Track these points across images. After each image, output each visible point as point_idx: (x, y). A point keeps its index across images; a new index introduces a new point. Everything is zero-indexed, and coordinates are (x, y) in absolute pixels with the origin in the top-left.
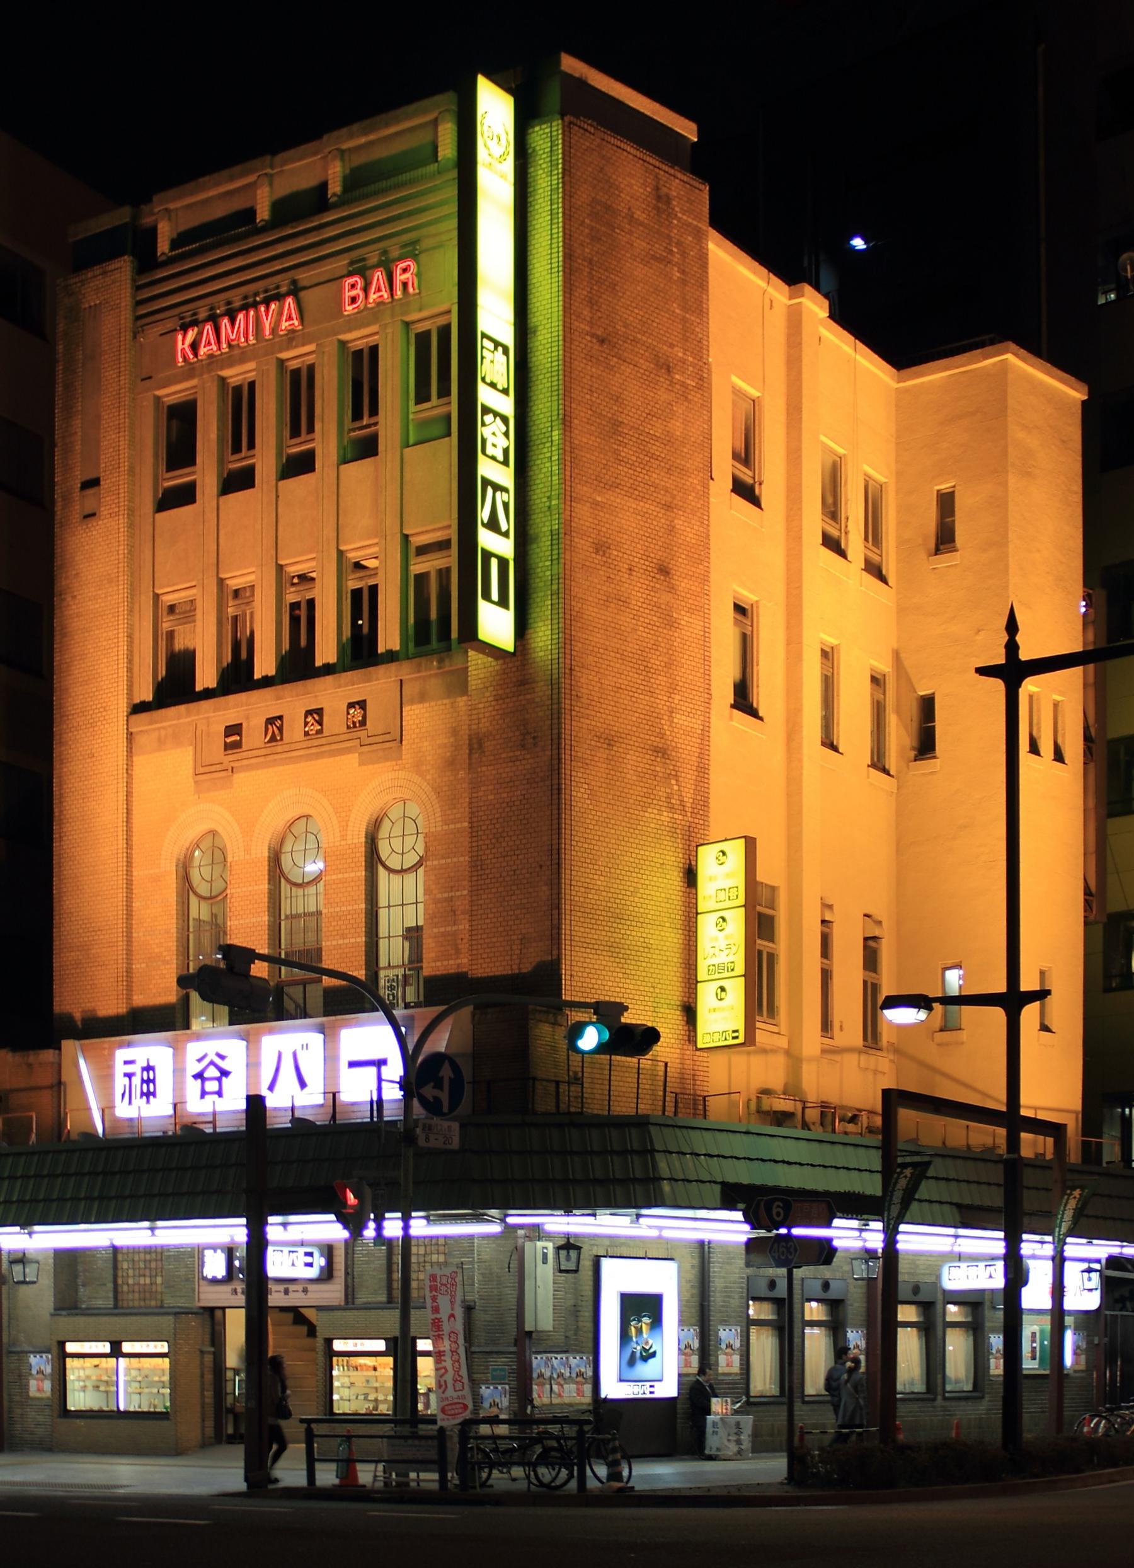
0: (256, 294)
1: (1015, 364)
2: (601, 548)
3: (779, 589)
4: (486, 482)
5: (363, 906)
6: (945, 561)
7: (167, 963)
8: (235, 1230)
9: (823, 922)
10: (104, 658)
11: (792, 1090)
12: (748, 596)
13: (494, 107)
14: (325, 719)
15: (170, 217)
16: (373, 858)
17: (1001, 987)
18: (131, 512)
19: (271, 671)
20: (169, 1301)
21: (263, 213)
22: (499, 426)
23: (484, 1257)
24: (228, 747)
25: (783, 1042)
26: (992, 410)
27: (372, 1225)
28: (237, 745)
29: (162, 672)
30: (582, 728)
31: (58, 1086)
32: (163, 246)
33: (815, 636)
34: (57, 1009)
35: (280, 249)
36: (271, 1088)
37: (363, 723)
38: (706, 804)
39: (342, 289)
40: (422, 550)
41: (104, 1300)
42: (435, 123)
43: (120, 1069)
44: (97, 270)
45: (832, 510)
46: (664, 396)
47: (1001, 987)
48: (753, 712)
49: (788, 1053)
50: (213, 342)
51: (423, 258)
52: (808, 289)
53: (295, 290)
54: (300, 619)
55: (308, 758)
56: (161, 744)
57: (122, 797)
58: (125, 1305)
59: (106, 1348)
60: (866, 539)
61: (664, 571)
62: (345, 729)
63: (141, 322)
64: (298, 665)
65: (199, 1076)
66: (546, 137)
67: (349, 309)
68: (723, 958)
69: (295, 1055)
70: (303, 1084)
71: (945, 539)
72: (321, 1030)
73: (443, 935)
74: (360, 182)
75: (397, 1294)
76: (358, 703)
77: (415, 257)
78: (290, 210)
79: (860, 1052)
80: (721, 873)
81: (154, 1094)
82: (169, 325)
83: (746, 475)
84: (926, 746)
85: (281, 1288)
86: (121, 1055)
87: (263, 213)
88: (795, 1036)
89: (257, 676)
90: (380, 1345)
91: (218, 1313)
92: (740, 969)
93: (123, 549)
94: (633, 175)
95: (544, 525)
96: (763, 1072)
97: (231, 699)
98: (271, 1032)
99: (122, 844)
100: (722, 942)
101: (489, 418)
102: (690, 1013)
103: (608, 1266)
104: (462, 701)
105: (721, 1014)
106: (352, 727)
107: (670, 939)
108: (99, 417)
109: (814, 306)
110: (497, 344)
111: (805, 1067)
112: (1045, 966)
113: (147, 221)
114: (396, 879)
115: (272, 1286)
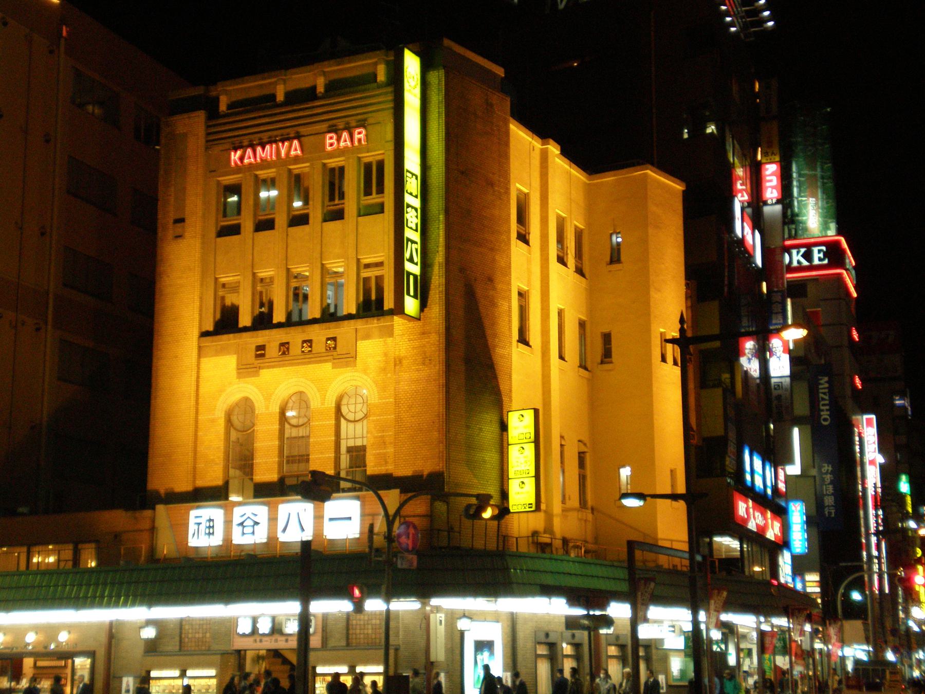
0: (277, 136)
1: (652, 174)
4: (408, 240)
5: (333, 438)
7: (216, 464)
10: (185, 308)
11: (549, 529)
14: (314, 345)
15: (226, 95)
18: (203, 236)
20: (215, 647)
21: (280, 97)
22: (413, 213)
28: (263, 355)
29: (218, 316)
32: (223, 107)
33: (555, 305)
36: (284, 530)
37: (335, 348)
39: (324, 139)
42: (376, 64)
44: (185, 116)
51: (369, 128)
52: (551, 141)
53: (298, 137)
59: (177, 673)
62: (324, 350)
63: (210, 143)
65: (241, 524)
66: (437, 77)
70: (303, 530)
73: (378, 454)
74: (336, 87)
77: (364, 127)
81: (213, 533)
82: (227, 146)
84: (607, 354)
86: (193, 513)
87: (280, 97)
89: (275, 321)
91: (242, 653)
97: (260, 333)
98: (283, 502)
101: (409, 209)
106: (328, 349)
108: (185, 188)
109: (554, 149)
110: (413, 174)
113: (214, 94)
114: (351, 425)
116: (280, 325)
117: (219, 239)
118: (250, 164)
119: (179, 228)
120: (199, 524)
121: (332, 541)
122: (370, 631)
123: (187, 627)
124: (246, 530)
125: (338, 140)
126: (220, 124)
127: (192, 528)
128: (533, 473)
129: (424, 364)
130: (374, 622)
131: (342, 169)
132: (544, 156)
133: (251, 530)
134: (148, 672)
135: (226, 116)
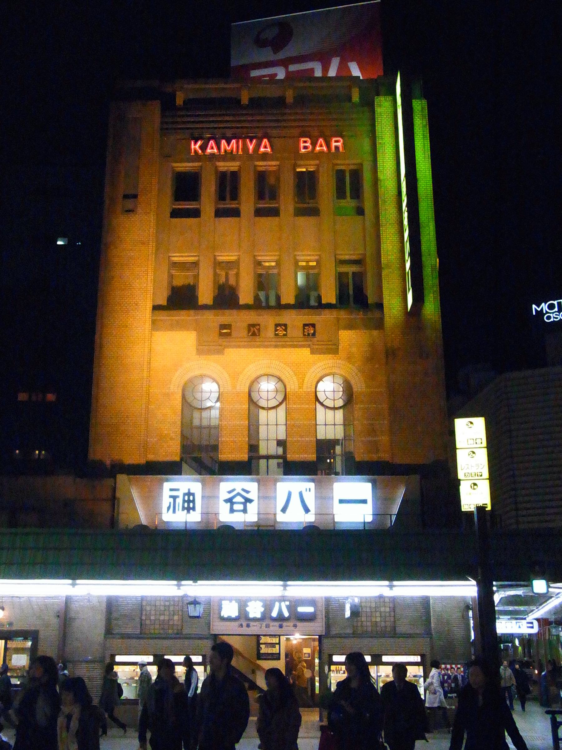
8: (467, 589)
19: (292, 301)
23: (437, 609)
28: (229, 334)
31: (113, 500)
36: (284, 510)
37: (314, 334)
50: (268, 146)
51: (346, 138)
53: (266, 136)
55: (276, 346)
58: (147, 632)
63: (164, 130)
65: (230, 501)
67: (303, 151)
69: (301, 494)
73: (370, 442)
76: (311, 324)
85: (277, 624)
86: (167, 486)
87: (245, 100)
90: (418, 659)
92: (486, 474)
113: (169, 90)
116: (247, 307)
117: (172, 219)
118: (213, 155)
119: (129, 204)
121: (168, 522)
122: (378, 619)
123: (148, 608)
124: (236, 507)
125: (314, 144)
126: (198, 116)
127: (166, 501)
130: (382, 609)
131: (235, 175)
133: (241, 507)
134: (113, 656)
135: (180, 109)
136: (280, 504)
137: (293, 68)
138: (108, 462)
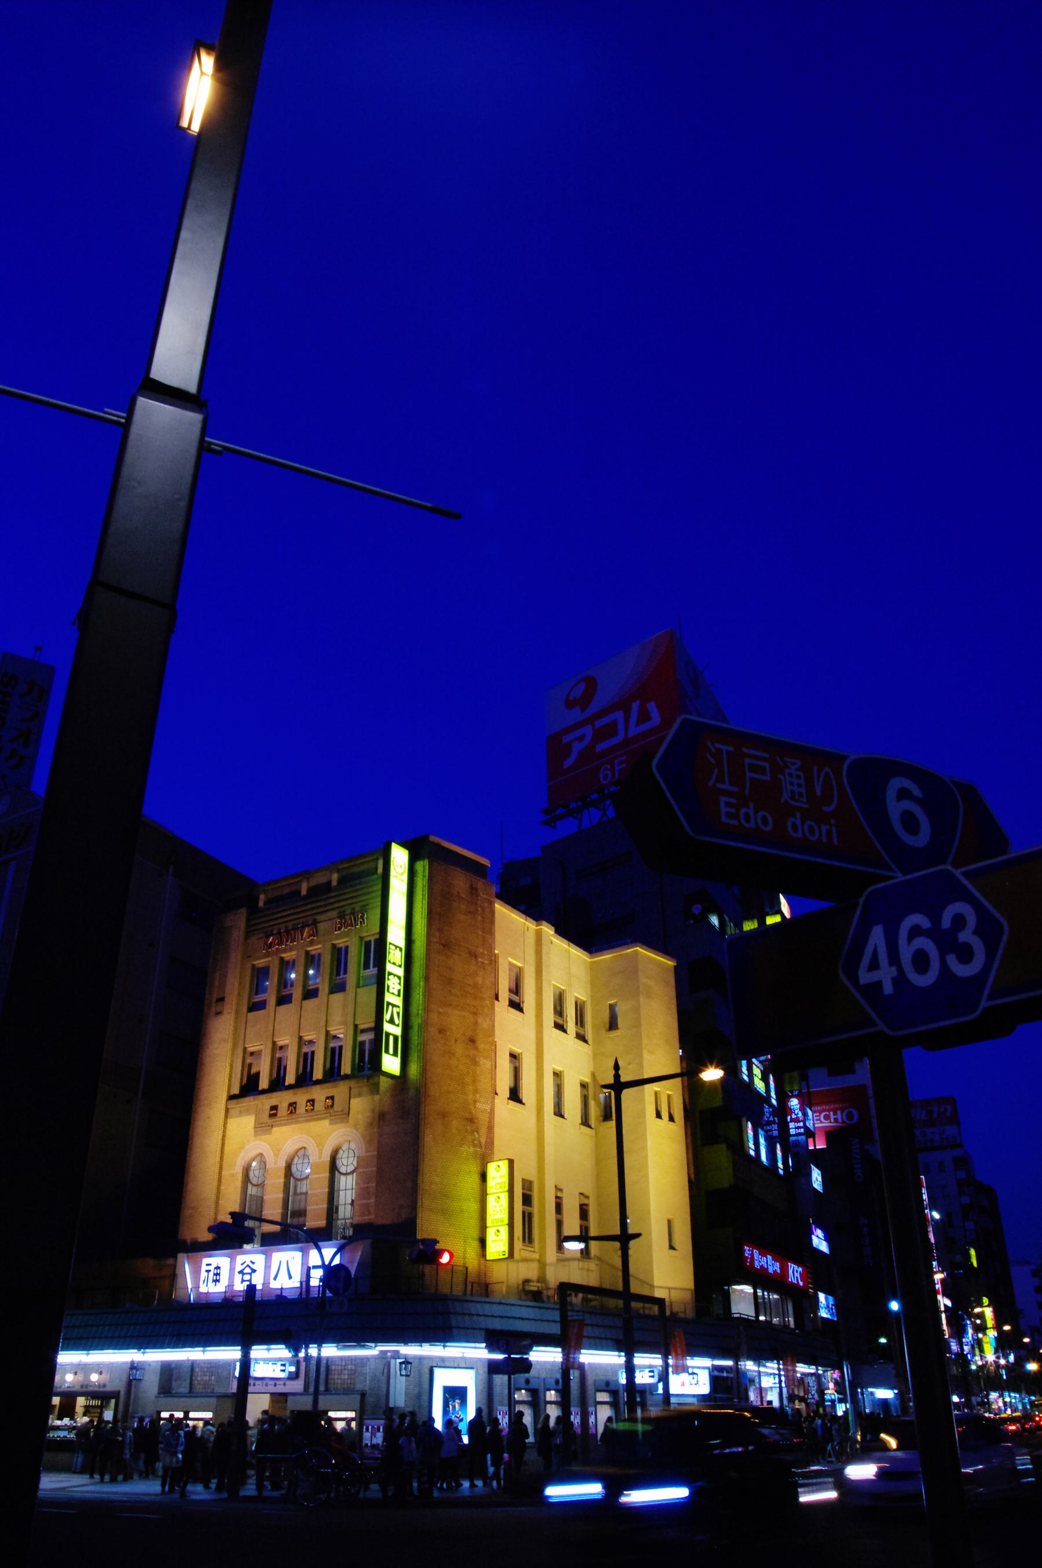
2: (441, 1031)
3: (533, 1047)
4: (389, 1004)
6: (614, 1034)
8: (231, 1354)
9: (557, 1197)
11: (542, 1279)
12: (517, 1050)
13: (399, 856)
16: (333, 1167)
17: (617, 1231)
18: (237, 1012)
24: (271, 1116)
25: (536, 1256)
26: (632, 971)
27: (303, 1351)
28: (275, 1115)
29: (245, 1081)
30: (430, 1110)
32: (261, 904)
34: (179, 1237)
35: (292, 911)
36: (275, 1279)
37: (332, 1106)
38: (492, 1143)
40: (363, 1031)
41: (184, 1389)
42: (377, 859)
43: (204, 1268)
45: (559, 1011)
46: (473, 968)
47: (617, 1231)
48: (520, 1101)
49: (539, 1261)
52: (544, 923)
54: (306, 1060)
55: (307, 1121)
56: (241, 1114)
57: (220, 1137)
60: (577, 1023)
61: (472, 1041)
63: (248, 935)
64: (304, 1079)
66: (422, 866)
68: (498, 1216)
70: (290, 1277)
71: (613, 1025)
72: (301, 1250)
75: (312, 1389)
78: (313, 891)
79: (579, 1260)
80: (497, 1174)
81: (219, 1281)
83: (516, 998)
85: (273, 1382)
86: (205, 1261)
87: (304, 892)
88: (543, 1253)
89: (260, 1088)
93: (231, 1028)
94: (460, 881)
95: (416, 1021)
96: (525, 1271)
97: (274, 1094)
99: (218, 1159)
100: (497, 1209)
101: (391, 977)
102: (483, 1242)
103: (438, 1372)
104: (377, 1097)
105: (497, 1245)
106: (327, 1108)
107: (474, 1206)
109: (548, 930)
110: (397, 947)
111: (548, 1268)
112: (670, 1217)
115: (251, 1382)
117: (250, 1014)
120: (208, 1271)
128: (506, 1221)
129: (402, 1118)
130: (350, 1367)
132: (539, 936)
134: (159, 1413)
136: (272, 1276)
137: (598, 723)
138: (189, 1241)
